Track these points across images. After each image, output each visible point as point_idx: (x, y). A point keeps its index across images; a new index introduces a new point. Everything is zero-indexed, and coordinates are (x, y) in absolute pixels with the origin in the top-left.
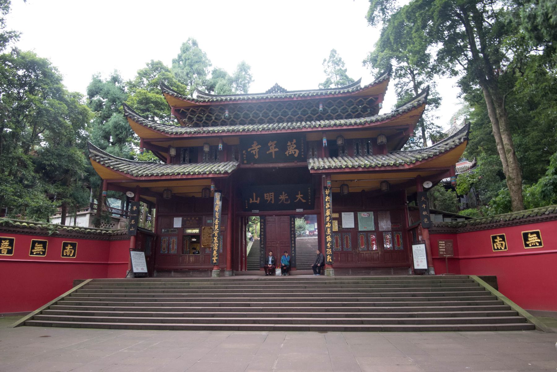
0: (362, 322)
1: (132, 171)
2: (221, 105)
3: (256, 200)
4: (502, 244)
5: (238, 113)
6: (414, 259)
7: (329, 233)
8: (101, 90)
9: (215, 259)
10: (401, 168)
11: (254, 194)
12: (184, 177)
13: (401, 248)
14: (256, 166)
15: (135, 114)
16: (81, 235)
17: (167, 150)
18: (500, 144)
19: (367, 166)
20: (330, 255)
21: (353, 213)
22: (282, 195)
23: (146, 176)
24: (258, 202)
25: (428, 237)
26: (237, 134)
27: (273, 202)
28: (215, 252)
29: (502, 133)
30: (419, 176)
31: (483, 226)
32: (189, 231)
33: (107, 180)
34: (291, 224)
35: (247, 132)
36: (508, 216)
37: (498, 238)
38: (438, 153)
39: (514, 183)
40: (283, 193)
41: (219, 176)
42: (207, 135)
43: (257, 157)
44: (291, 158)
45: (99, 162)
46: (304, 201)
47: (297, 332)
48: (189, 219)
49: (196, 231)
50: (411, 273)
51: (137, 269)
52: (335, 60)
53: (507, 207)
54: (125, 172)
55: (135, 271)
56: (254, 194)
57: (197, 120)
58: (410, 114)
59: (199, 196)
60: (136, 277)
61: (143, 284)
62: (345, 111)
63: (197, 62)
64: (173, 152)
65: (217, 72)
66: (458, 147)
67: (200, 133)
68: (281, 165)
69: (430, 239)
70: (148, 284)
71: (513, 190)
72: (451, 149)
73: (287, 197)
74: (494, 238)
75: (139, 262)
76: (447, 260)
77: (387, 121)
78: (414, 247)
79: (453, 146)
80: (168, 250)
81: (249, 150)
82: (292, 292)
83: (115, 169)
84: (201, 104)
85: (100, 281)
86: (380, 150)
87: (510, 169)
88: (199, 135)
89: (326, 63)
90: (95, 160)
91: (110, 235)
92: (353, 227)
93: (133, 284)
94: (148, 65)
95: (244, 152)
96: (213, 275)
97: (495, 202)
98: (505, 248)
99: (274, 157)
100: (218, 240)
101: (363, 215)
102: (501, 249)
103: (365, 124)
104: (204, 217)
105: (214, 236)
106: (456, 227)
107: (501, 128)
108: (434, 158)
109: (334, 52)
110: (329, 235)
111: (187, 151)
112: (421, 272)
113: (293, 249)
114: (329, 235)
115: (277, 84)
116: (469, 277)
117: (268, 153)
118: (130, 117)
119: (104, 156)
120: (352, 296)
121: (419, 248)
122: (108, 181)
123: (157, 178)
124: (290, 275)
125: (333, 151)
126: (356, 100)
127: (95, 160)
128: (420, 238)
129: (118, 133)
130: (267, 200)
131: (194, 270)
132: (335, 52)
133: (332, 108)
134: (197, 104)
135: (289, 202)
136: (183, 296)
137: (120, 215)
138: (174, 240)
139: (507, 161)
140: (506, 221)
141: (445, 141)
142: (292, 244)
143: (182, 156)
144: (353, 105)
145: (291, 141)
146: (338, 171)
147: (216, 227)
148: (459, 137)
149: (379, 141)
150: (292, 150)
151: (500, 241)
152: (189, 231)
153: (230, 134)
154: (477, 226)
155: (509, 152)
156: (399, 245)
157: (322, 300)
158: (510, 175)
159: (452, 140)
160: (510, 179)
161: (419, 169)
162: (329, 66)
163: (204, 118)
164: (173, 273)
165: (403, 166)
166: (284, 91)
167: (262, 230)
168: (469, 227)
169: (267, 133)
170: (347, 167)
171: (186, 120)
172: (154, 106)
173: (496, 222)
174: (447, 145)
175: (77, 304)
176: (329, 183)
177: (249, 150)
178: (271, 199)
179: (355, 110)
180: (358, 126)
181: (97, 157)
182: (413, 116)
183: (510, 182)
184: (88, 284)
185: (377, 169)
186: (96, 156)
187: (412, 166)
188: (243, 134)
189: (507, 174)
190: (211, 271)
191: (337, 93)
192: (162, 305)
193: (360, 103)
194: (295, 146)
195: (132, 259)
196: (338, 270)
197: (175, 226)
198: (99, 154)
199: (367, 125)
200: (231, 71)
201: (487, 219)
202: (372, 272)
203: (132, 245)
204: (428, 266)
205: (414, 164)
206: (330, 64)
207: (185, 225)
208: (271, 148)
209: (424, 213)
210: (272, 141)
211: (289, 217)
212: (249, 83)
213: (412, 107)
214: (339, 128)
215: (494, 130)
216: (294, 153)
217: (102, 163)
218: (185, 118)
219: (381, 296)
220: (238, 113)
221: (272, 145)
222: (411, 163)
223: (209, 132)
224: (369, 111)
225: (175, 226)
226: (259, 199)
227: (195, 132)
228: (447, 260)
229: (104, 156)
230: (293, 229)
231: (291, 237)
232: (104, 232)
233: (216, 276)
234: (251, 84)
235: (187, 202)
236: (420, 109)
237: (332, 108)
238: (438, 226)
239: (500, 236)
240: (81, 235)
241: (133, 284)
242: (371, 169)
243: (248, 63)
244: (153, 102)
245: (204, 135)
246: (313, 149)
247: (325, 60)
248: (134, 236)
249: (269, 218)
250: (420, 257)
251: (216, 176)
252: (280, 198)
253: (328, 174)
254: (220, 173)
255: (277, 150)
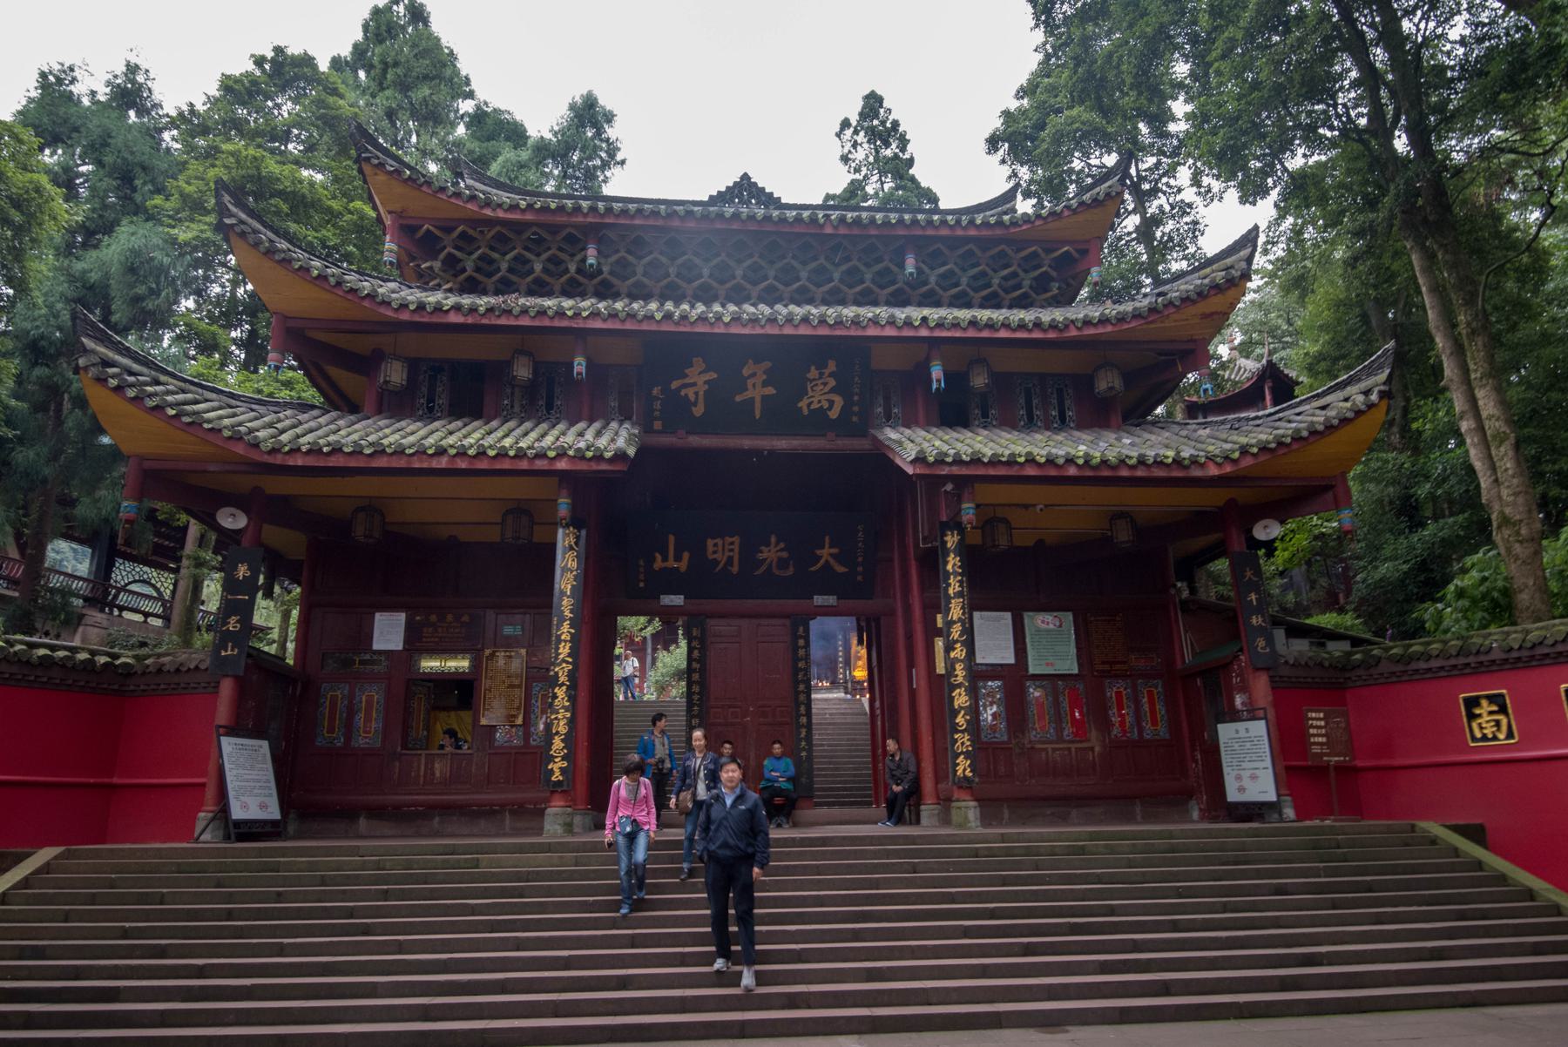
0: (1165, 989)
1: (251, 431)
2: (575, 226)
3: (678, 558)
4: (1498, 723)
5: (630, 258)
6: (1226, 770)
7: (960, 679)
8: (76, 129)
9: (557, 767)
10: (1196, 472)
11: (672, 539)
12: (462, 464)
13: (1163, 731)
14: (695, 441)
15: (258, 226)
16: (14, 669)
17: (367, 364)
18: (1470, 415)
19: (1095, 462)
20: (967, 755)
21: (1008, 615)
22: (768, 545)
23: (309, 452)
24: (683, 565)
25: (1270, 698)
26: (645, 327)
27: (735, 569)
28: (558, 743)
29: (1474, 384)
30: (1232, 502)
31: (1434, 664)
32: (430, 664)
33: (142, 458)
34: (796, 648)
35: (677, 324)
36: (1496, 638)
37: (1484, 703)
38: (1305, 434)
39: (1518, 533)
40: (773, 539)
41: (594, 466)
42: (537, 323)
43: (698, 411)
44: (818, 422)
45: (119, 389)
46: (841, 569)
47: (914, 1035)
48: (433, 618)
49: (460, 664)
50: (1195, 815)
51: (245, 806)
52: (875, 123)
53: (1500, 607)
54: (226, 433)
55: (237, 813)
56: (672, 539)
57: (478, 270)
58: (1203, 307)
59: (493, 535)
60: (242, 838)
61: (289, 867)
62: (981, 282)
63: (426, 77)
64: (395, 374)
65: (489, 121)
66: (1363, 418)
67: (508, 312)
68: (781, 444)
69: (1276, 704)
70: (312, 867)
71: (1517, 558)
72: (1344, 421)
73: (785, 554)
74: (1472, 703)
75: (248, 779)
76: (1332, 774)
77: (1133, 324)
78: (1227, 732)
79: (1350, 415)
80: (348, 738)
81: (675, 385)
82: (876, 884)
83: (186, 419)
84: (501, 214)
85: (97, 854)
86: (1099, 413)
87: (1505, 492)
88: (503, 321)
89: (849, 132)
90: (102, 380)
91: (127, 672)
92: (1012, 661)
93: (247, 867)
94: (259, 61)
95: (656, 391)
96: (547, 827)
97: (1461, 594)
98: (1510, 735)
99: (758, 414)
100: (572, 698)
101: (1040, 622)
102: (1495, 738)
103: (1067, 326)
104: (490, 614)
105: (554, 681)
106: (1344, 669)
107: (1472, 366)
108: (1295, 446)
109: (873, 103)
110: (959, 686)
111: (464, 379)
112: (1252, 811)
113: (803, 732)
114: (959, 686)
115: (745, 177)
116: (1413, 826)
117: (738, 399)
118: (243, 235)
119: (136, 367)
120: (1084, 895)
121: (1242, 734)
122: (147, 465)
123: (353, 463)
124: (795, 825)
125: (954, 411)
126: (1019, 250)
127: (102, 380)
128: (1238, 701)
129: (141, 290)
130: (716, 562)
131: (447, 809)
132: (880, 100)
133: (942, 270)
134: (488, 212)
135: (790, 571)
136: (473, 910)
137: (86, 599)
138: (372, 695)
139: (1493, 468)
140: (1511, 649)
141: (1318, 396)
142: (799, 716)
143: (424, 390)
144: (1007, 266)
145: (821, 366)
146: (1002, 471)
147: (564, 650)
148: (1363, 385)
149: (1102, 385)
150: (821, 396)
151: (1491, 713)
152: (430, 664)
153: (618, 326)
154: (1414, 666)
155: (1501, 442)
156: (1154, 723)
157: (992, 914)
158: (1508, 511)
159: (1340, 395)
160: (1505, 521)
161: (1244, 478)
162: (855, 145)
163: (504, 266)
164: (363, 823)
165: (1202, 466)
166: (769, 200)
167: (695, 665)
168: (1385, 667)
169: (746, 331)
170: (1031, 460)
171: (437, 265)
172: (285, 208)
173: (1478, 652)
174: (1323, 408)
175: (22, 953)
176: (968, 511)
177: (675, 385)
178: (730, 559)
179: (1011, 283)
180: (1045, 331)
181: (111, 371)
182: (1212, 314)
183: (1506, 532)
184: (46, 868)
185: (1124, 473)
186: (107, 363)
187: (1228, 469)
188: (665, 327)
189: (1496, 507)
190: (541, 813)
191: (964, 223)
192: (400, 948)
193: (1032, 262)
194: (832, 383)
195: (227, 766)
196: (991, 807)
197: (376, 646)
198: (118, 358)
199: (1073, 333)
200: (542, 119)
201: (1445, 642)
202: (1074, 812)
203: (223, 714)
204: (1279, 795)
205: (1235, 461)
206: (861, 138)
207: (417, 643)
208: (750, 382)
209: (1254, 621)
210: (757, 361)
211: (787, 622)
212: (605, 165)
213: (1211, 287)
214: (985, 334)
215: (1447, 372)
216: (826, 405)
217: (131, 393)
218: (435, 258)
219: (1179, 893)
220: (630, 258)
221: (753, 375)
222: (1227, 458)
223: (542, 313)
224: (1055, 291)
225: (376, 646)
226: (686, 555)
227: (490, 310)
228: (1332, 774)
229: (136, 367)
230: (801, 665)
231: (798, 693)
232: (103, 660)
233: (559, 830)
234: (615, 173)
235: (449, 563)
236: (1232, 293)
237: (942, 270)
238: (1295, 665)
239: (1492, 699)
240: (14, 669)
241: (247, 867)
242: (1106, 473)
243: (605, 101)
244: (281, 194)
245: (525, 322)
246: (887, 399)
247: (845, 124)
248: (236, 677)
249: (718, 626)
250: (1249, 762)
251: (582, 466)
252: (761, 556)
253: (963, 482)
254: (599, 457)
255: (770, 391)
